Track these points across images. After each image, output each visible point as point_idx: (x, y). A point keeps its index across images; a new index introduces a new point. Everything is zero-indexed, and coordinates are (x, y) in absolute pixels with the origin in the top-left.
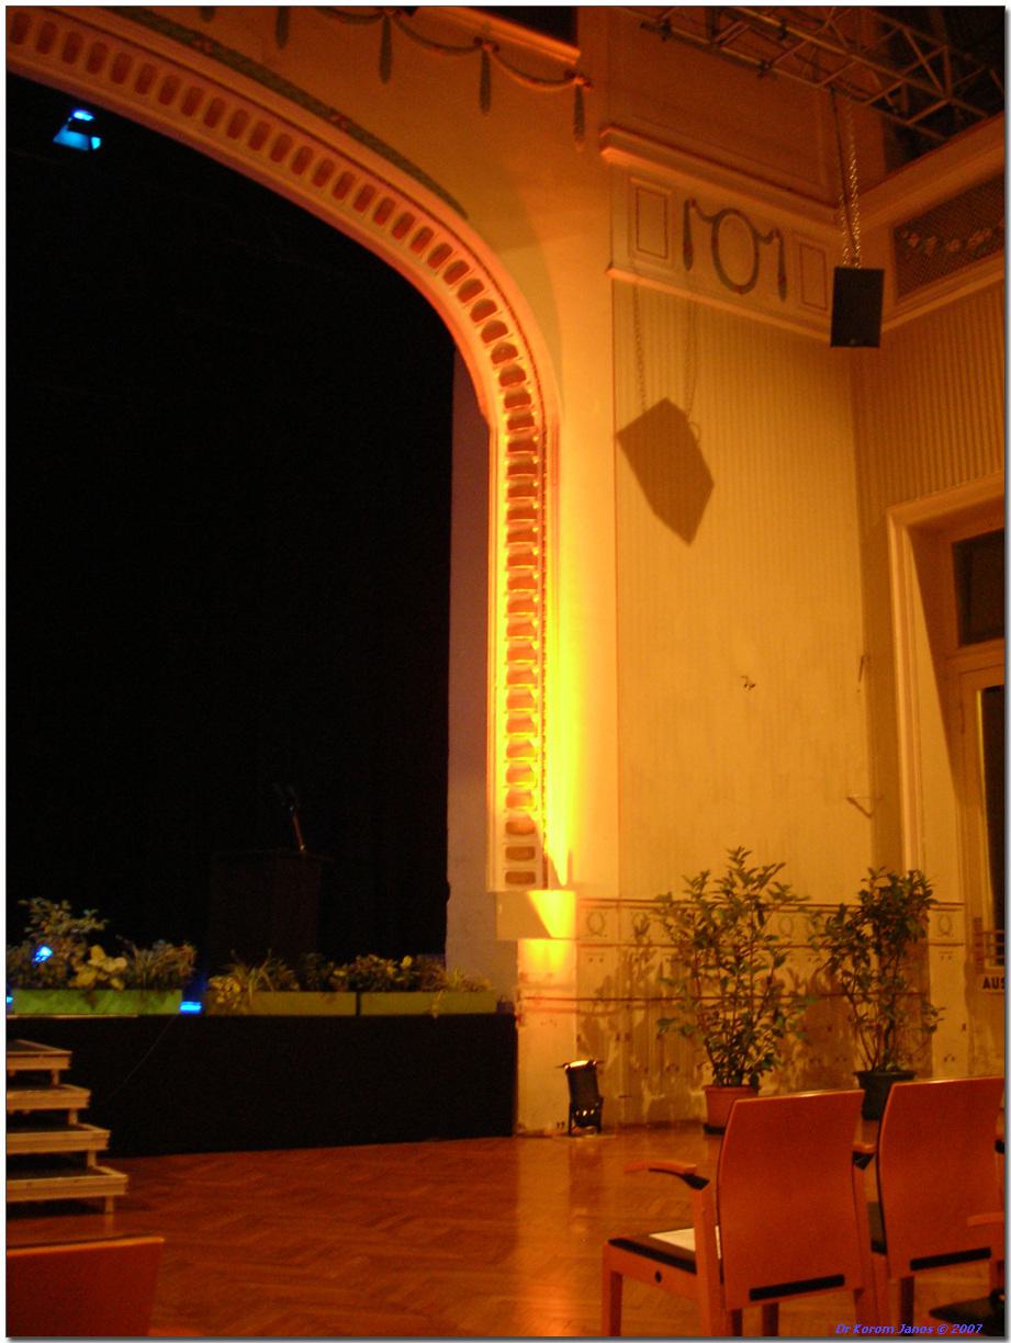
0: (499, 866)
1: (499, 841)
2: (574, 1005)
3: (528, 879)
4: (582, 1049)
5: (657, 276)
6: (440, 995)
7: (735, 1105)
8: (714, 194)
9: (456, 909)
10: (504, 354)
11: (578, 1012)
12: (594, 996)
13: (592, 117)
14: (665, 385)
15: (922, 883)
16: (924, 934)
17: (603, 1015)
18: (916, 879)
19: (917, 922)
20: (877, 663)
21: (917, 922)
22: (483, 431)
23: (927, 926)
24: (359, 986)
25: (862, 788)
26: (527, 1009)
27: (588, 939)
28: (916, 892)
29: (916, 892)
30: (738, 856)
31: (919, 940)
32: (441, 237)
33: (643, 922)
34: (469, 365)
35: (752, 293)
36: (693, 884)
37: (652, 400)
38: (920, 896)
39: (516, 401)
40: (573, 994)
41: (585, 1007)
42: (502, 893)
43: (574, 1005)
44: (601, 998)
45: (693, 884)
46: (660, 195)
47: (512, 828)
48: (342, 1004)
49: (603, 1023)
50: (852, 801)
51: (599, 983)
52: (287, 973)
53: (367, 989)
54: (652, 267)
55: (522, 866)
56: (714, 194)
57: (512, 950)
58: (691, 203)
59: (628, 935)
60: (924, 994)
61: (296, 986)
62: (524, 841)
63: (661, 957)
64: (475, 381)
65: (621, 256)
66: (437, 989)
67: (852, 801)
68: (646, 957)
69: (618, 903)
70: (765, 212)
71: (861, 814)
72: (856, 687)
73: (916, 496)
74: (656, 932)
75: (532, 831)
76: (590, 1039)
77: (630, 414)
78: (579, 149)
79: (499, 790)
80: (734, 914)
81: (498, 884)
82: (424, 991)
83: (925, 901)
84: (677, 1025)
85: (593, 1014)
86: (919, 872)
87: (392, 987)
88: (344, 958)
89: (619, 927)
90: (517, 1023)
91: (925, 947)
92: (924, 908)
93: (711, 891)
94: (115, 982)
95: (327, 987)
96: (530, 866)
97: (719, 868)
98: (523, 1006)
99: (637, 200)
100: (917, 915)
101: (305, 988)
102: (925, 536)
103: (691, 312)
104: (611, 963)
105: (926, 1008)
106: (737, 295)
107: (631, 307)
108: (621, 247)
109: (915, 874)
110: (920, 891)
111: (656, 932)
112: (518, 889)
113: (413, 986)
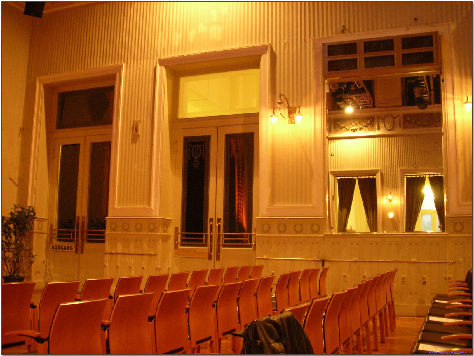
7: (197, 288)
15: (33, 211)
16: (32, 229)
18: (31, 209)
19: (30, 224)
21: (30, 224)
23: (33, 226)
28: (30, 214)
29: (30, 214)
31: (30, 231)
38: (31, 215)
60: (30, 250)
61: (405, 120)
73: (48, 74)
79: (287, 308)
82: (50, 186)
83: (33, 217)
84: (143, 292)
86: (32, 207)
90: (161, 59)
91: (32, 233)
92: (33, 220)
100: (30, 222)
102: (49, 88)
105: (31, 255)
109: (31, 207)
110: (32, 214)
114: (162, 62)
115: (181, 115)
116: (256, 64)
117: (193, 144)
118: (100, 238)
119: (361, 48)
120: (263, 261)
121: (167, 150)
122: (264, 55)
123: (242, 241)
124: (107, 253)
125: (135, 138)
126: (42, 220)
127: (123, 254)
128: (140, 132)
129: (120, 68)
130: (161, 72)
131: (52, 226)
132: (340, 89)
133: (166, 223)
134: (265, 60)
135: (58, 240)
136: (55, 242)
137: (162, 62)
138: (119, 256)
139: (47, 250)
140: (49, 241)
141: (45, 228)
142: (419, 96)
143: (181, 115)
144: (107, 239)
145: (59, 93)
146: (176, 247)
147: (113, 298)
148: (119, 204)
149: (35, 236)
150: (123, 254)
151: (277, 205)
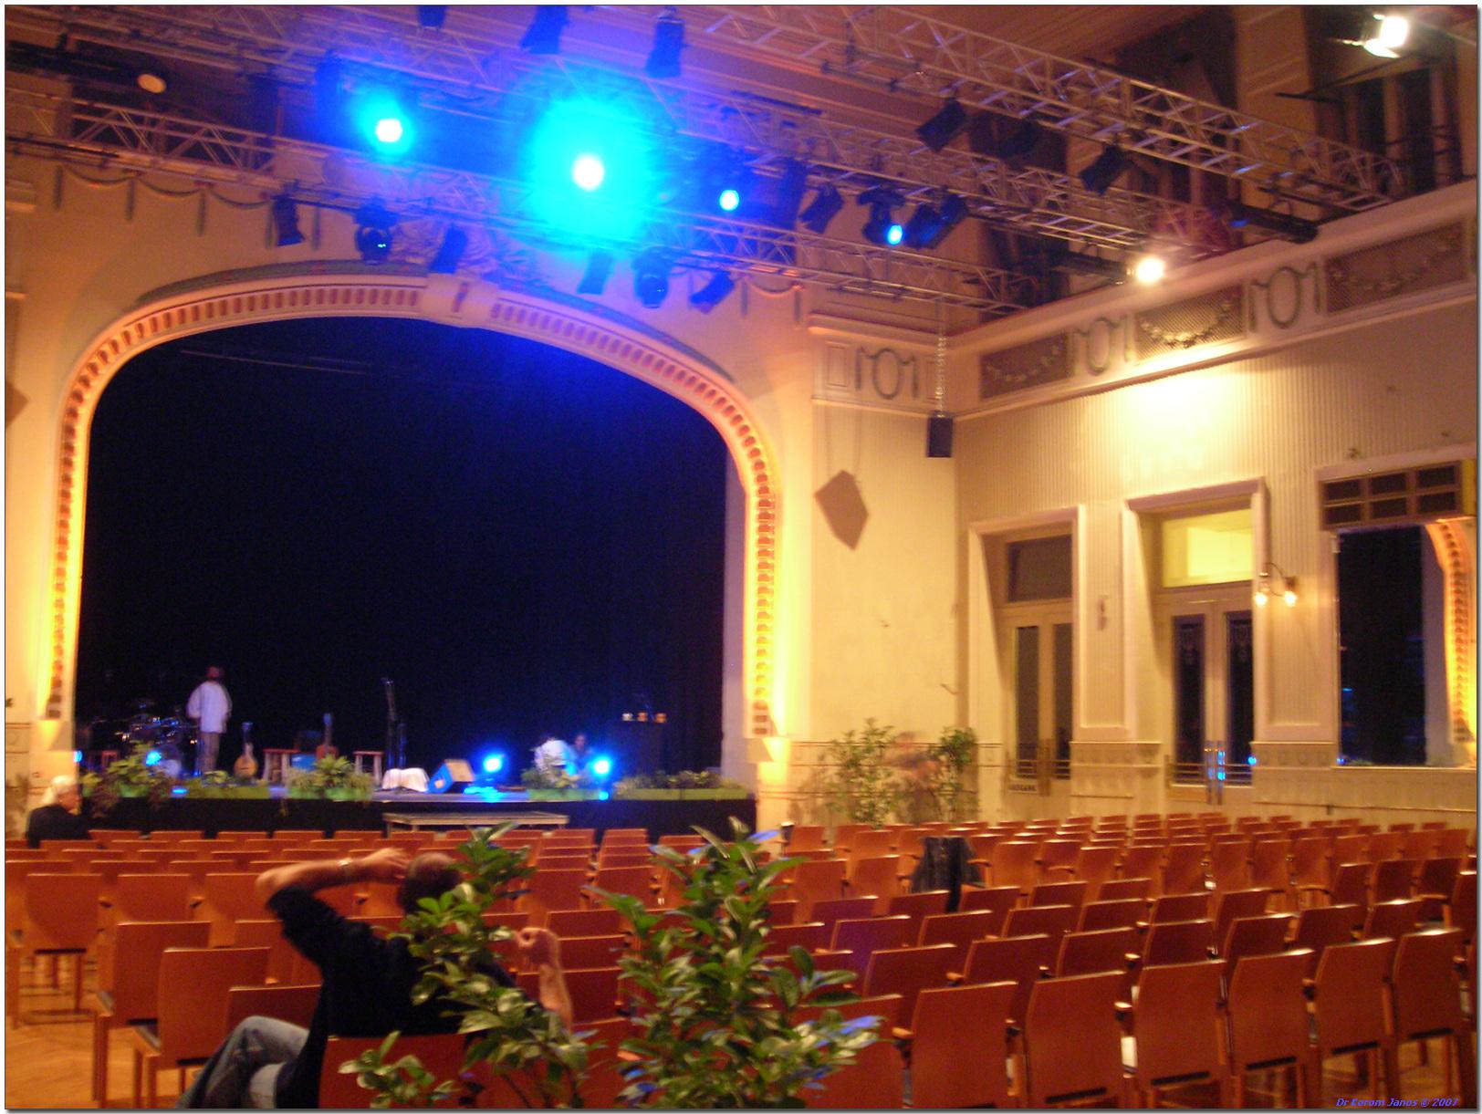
0: (749, 726)
1: (750, 712)
2: (786, 795)
3: (762, 731)
4: (791, 817)
5: (840, 398)
6: (719, 790)
7: (1232, 927)
8: (874, 341)
9: (727, 745)
10: (759, 465)
11: (787, 799)
12: (796, 791)
13: (806, 307)
14: (844, 463)
17: (800, 800)
20: (961, 609)
22: (742, 495)
24: (683, 785)
25: (951, 678)
26: (763, 798)
27: (795, 764)
30: (870, 721)
32: (721, 394)
33: (1127, 133)
34: (735, 459)
35: (898, 399)
36: (846, 734)
37: (835, 473)
39: (762, 478)
40: (785, 790)
41: (792, 796)
42: (751, 739)
43: (786, 795)
44: (801, 791)
45: (846, 734)
46: (843, 348)
47: (758, 706)
48: (674, 795)
49: (801, 804)
50: (944, 686)
51: (799, 784)
52: (648, 780)
53: (684, 788)
54: (839, 394)
55: (762, 725)
56: (874, 341)
57: (754, 768)
58: (862, 350)
59: (815, 761)
62: (761, 713)
63: (833, 771)
64: (739, 469)
65: (820, 391)
66: (717, 788)
67: (944, 686)
68: (823, 771)
69: (809, 744)
70: (904, 346)
71: (949, 693)
72: (950, 623)
74: (830, 759)
75: (765, 708)
76: (795, 812)
77: (823, 480)
78: (797, 328)
80: (869, 750)
81: (749, 734)
85: (795, 800)
87: (697, 786)
88: (675, 772)
89: (811, 756)
91: (977, 767)
93: (857, 738)
94: (573, 786)
95: (666, 786)
96: (764, 724)
97: (860, 728)
98: (760, 796)
99: (829, 351)
101: (658, 787)
102: (989, 541)
103: (859, 416)
104: (804, 776)
106: (885, 401)
107: (826, 419)
108: (819, 381)
111: (830, 759)
112: (758, 737)
113: (707, 785)
114: (1133, 505)
115: (1173, 578)
116: (1245, 504)
117: (1185, 626)
118: (1063, 772)
119: (1366, 488)
120: (1261, 807)
121: (1148, 638)
122: (1254, 494)
123: (1196, 775)
124: (1074, 796)
125: (1102, 623)
126: (991, 746)
127: (1095, 797)
128: (1107, 614)
129: (1074, 513)
130: (1130, 521)
131: (1007, 754)
132: (505, 883)
133: (1149, 751)
134: (1257, 499)
135: (1019, 776)
136: (1015, 780)
137: (1133, 505)
138: (1088, 800)
139: (1003, 792)
140: (1005, 779)
141: (998, 757)
142: (362, 895)
143: (1173, 578)
144: (1074, 774)
145: (1007, 544)
146: (1167, 786)
147: (139, 322)
148: (1090, 718)
149: (983, 771)
150: (1095, 797)
151: (1279, 724)
